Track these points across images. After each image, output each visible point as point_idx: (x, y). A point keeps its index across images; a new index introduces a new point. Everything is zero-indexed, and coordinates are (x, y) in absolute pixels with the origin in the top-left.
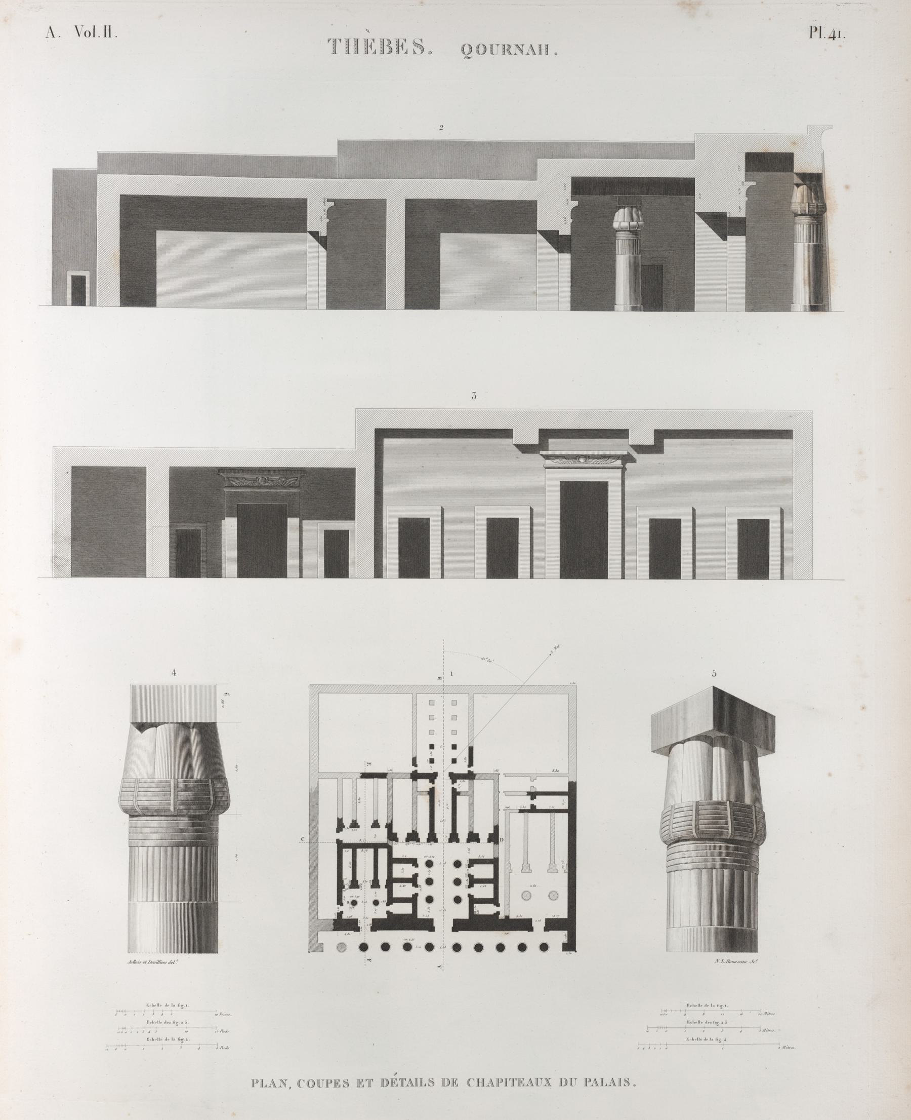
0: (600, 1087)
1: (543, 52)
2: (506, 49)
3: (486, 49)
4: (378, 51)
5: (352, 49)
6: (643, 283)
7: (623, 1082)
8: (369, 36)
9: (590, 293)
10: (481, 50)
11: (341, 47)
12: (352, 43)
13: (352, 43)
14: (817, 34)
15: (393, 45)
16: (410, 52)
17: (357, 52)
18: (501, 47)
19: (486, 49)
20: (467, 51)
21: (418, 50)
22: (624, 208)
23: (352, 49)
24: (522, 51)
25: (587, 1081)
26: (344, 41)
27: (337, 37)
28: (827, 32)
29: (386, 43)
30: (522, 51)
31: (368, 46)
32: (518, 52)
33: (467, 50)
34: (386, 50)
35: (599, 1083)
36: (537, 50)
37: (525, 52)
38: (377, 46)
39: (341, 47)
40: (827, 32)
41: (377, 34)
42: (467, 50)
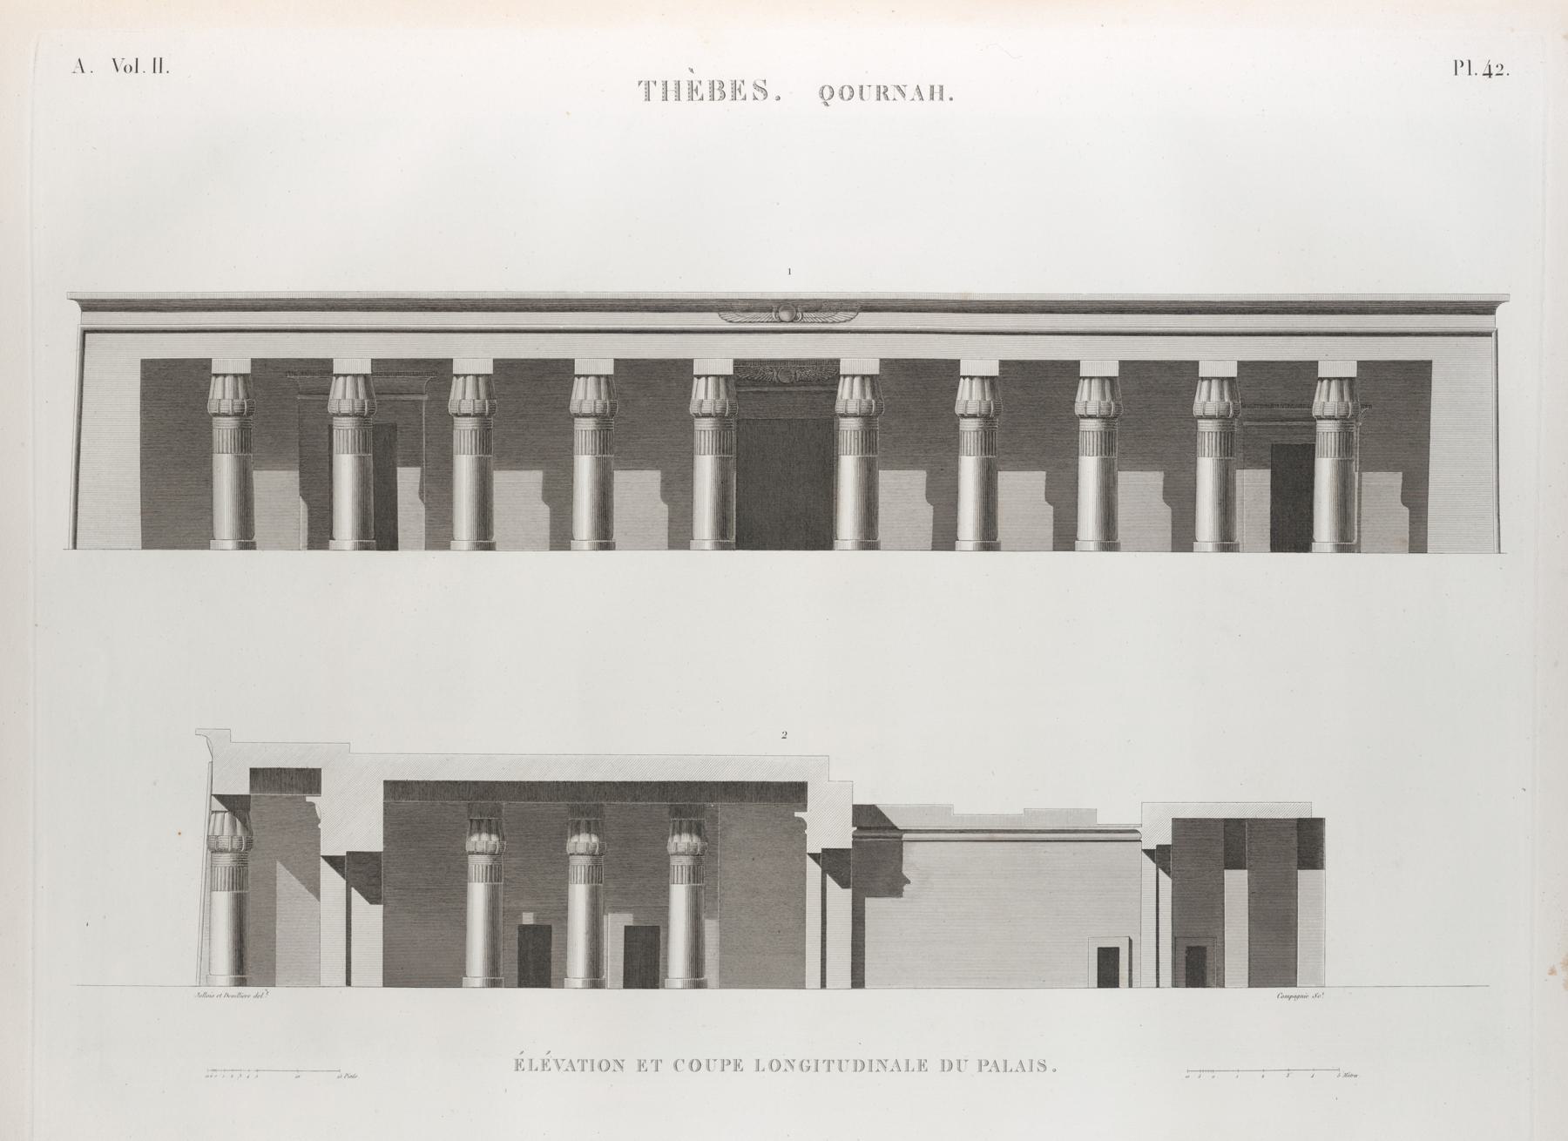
0: (1001, 1073)
1: (937, 96)
2: (882, 93)
3: (852, 92)
4: (707, 97)
5: (671, 95)
6: (724, 947)
7: (1035, 1065)
8: (694, 78)
9: (418, 962)
10: (847, 93)
11: (656, 92)
12: (671, 86)
13: (671, 86)
14: (1463, 70)
15: (728, 89)
16: (750, 97)
17: (678, 98)
18: (874, 90)
19: (852, 92)
20: (937, 93)
21: (760, 95)
22: (490, 832)
23: (671, 95)
24: (904, 95)
25: (980, 1065)
26: (659, 84)
27: (651, 79)
28: (1478, 67)
29: (717, 86)
30: (904, 95)
31: (693, 90)
32: (898, 96)
33: (827, 93)
34: (717, 94)
35: (1001, 1067)
36: (926, 94)
37: (908, 97)
38: (704, 90)
39: (656, 92)
40: (1478, 67)
41: (704, 75)
42: (827, 93)
